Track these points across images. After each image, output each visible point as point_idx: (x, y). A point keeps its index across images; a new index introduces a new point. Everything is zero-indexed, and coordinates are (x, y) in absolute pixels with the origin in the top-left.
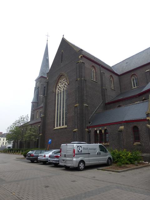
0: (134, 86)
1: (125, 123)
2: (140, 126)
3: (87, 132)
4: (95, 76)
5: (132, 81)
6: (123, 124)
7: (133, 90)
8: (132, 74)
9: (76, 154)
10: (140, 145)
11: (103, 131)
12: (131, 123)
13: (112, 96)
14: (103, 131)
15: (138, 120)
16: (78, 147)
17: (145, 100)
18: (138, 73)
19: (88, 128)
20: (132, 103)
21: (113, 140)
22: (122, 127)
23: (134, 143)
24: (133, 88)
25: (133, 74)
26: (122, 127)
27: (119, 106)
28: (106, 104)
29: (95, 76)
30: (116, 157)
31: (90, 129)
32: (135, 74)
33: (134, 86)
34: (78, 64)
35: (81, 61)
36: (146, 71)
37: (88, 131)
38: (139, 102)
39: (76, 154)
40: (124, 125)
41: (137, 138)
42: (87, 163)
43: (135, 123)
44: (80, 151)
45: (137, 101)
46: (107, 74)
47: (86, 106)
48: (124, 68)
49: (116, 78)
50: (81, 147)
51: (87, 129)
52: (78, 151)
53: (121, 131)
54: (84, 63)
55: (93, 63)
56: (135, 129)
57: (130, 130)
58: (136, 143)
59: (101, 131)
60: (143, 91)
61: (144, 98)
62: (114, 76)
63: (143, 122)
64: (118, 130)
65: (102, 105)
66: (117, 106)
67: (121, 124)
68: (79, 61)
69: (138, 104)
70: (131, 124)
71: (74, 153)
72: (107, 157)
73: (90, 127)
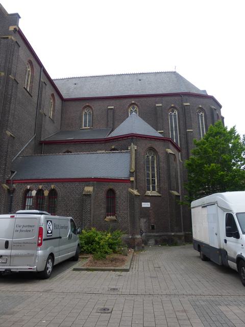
0: (85, 126)
1: (95, 182)
2: (119, 190)
3: (6, 191)
4: (29, 83)
5: (83, 116)
6: (91, 182)
7: (84, 130)
8: (130, 103)
9: (44, 240)
10: (115, 221)
11: (46, 193)
12: (104, 183)
13: (50, 132)
14: (46, 193)
15: (113, 179)
16: (48, 221)
17: (114, 149)
18: (96, 105)
19: (8, 182)
20: (92, 151)
21: (66, 210)
22: (89, 189)
23: (106, 217)
24: (83, 128)
25: (87, 104)
26: (89, 189)
27: (68, 152)
28: (41, 143)
29: (29, 83)
30: (84, 242)
31: (14, 185)
32: (91, 106)
33: (85, 126)
34: (5, 41)
35: (13, 38)
36: (109, 107)
37: (8, 190)
38: (104, 151)
39: (44, 240)
40: (93, 186)
41: (111, 210)
42: (58, 258)
43: (111, 183)
44: (50, 232)
45: (101, 150)
46: (49, 90)
47: (11, 135)
48: (71, 90)
49: (58, 101)
50: (51, 221)
51: (5, 186)
52: (48, 233)
53: (88, 195)
54: (19, 46)
55: (32, 56)
56: (111, 194)
57: (102, 195)
58: (109, 217)
59: (40, 192)
60: (110, 136)
61: (113, 147)
62: (57, 97)
63: (124, 184)
64: (84, 193)
65: (33, 142)
66: (64, 151)
67: (88, 183)
68: (10, 37)
69: (103, 154)
70: (104, 185)
71: (42, 237)
72: (77, 243)
73: (14, 181)
